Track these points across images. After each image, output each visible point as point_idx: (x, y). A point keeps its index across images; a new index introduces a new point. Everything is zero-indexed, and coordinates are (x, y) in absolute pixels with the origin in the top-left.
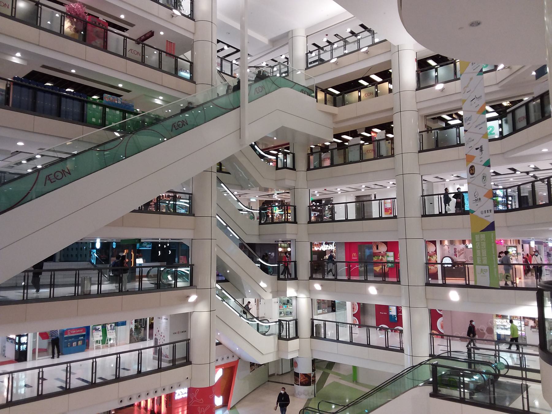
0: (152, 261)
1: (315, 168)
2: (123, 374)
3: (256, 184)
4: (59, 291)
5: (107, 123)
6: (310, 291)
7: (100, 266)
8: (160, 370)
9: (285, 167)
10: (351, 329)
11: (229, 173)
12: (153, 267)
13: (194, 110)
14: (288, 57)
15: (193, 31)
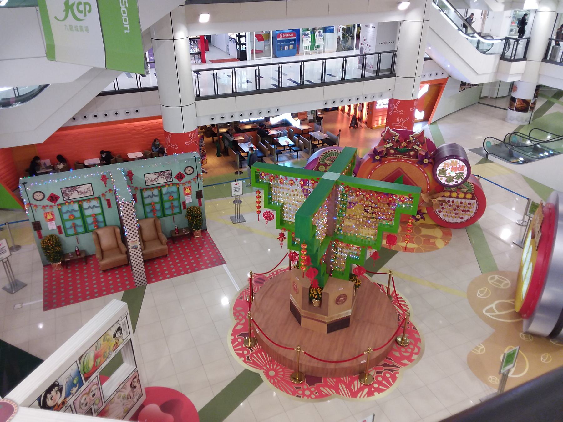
2: (328, 79)
8: (363, 78)
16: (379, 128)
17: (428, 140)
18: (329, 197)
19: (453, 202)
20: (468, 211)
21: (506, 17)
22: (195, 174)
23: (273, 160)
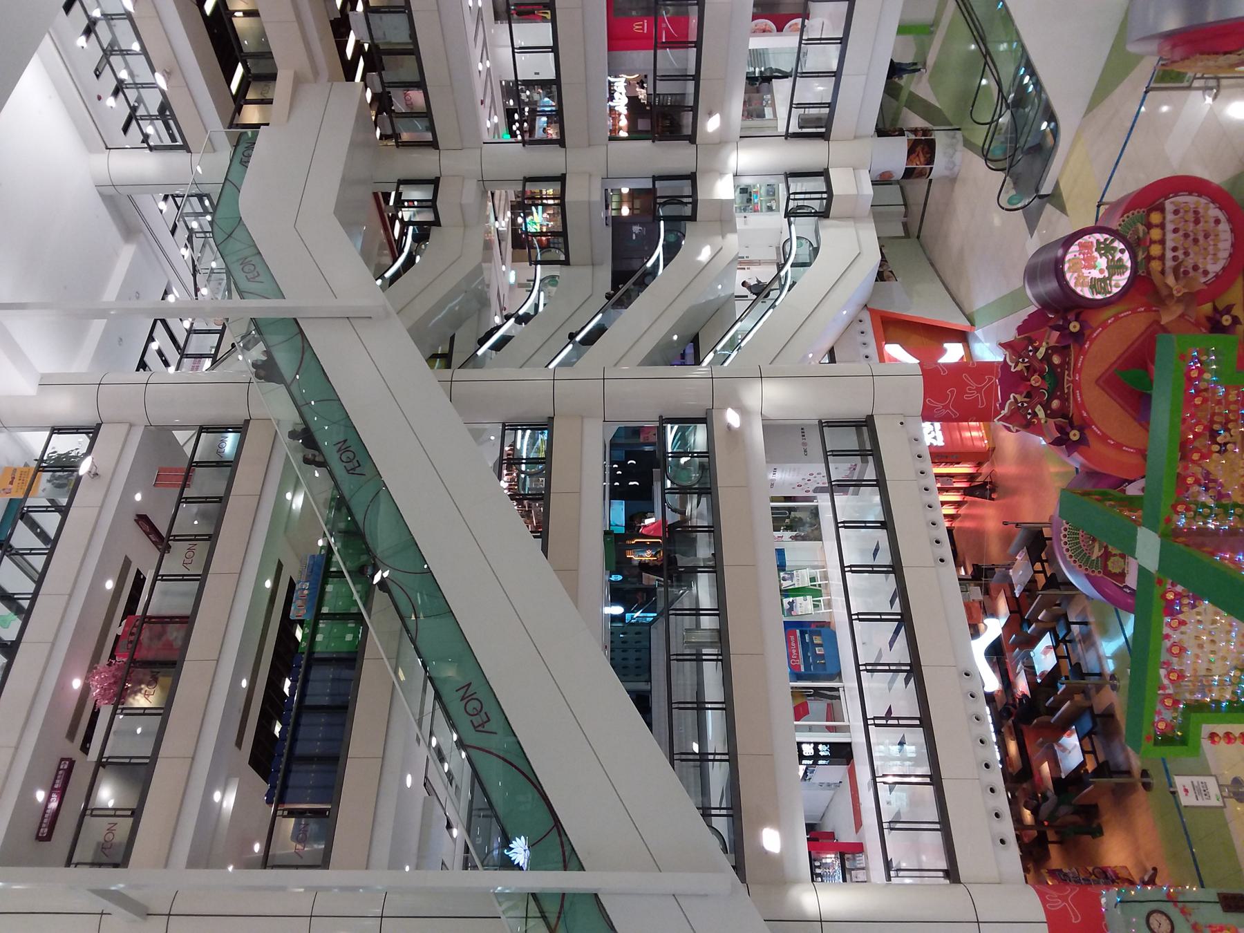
0: (650, 498)
1: (432, 128)
2: (885, 558)
3: (478, 271)
4: (713, 692)
5: (354, 610)
6: (721, 142)
7: (661, 605)
8: (880, 483)
9: (431, 204)
10: (812, 41)
11: (452, 338)
12: (664, 500)
13: (308, 418)
14: (162, 195)
15: (125, 427)
16: (991, 435)
17: (1020, 330)
18: (1213, 554)
19: (1175, 249)
20: (1196, 212)
21: (745, 223)
22: (1169, 908)
23: (1099, 688)
